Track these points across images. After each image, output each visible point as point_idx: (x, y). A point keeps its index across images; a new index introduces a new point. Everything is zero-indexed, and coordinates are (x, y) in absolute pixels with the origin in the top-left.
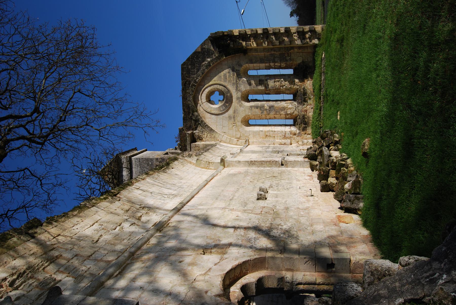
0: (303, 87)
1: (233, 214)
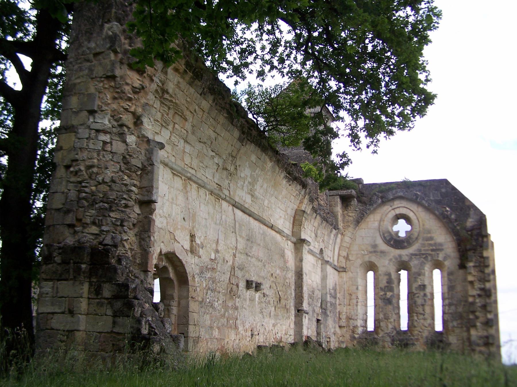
0: (416, 343)
1: (230, 257)
